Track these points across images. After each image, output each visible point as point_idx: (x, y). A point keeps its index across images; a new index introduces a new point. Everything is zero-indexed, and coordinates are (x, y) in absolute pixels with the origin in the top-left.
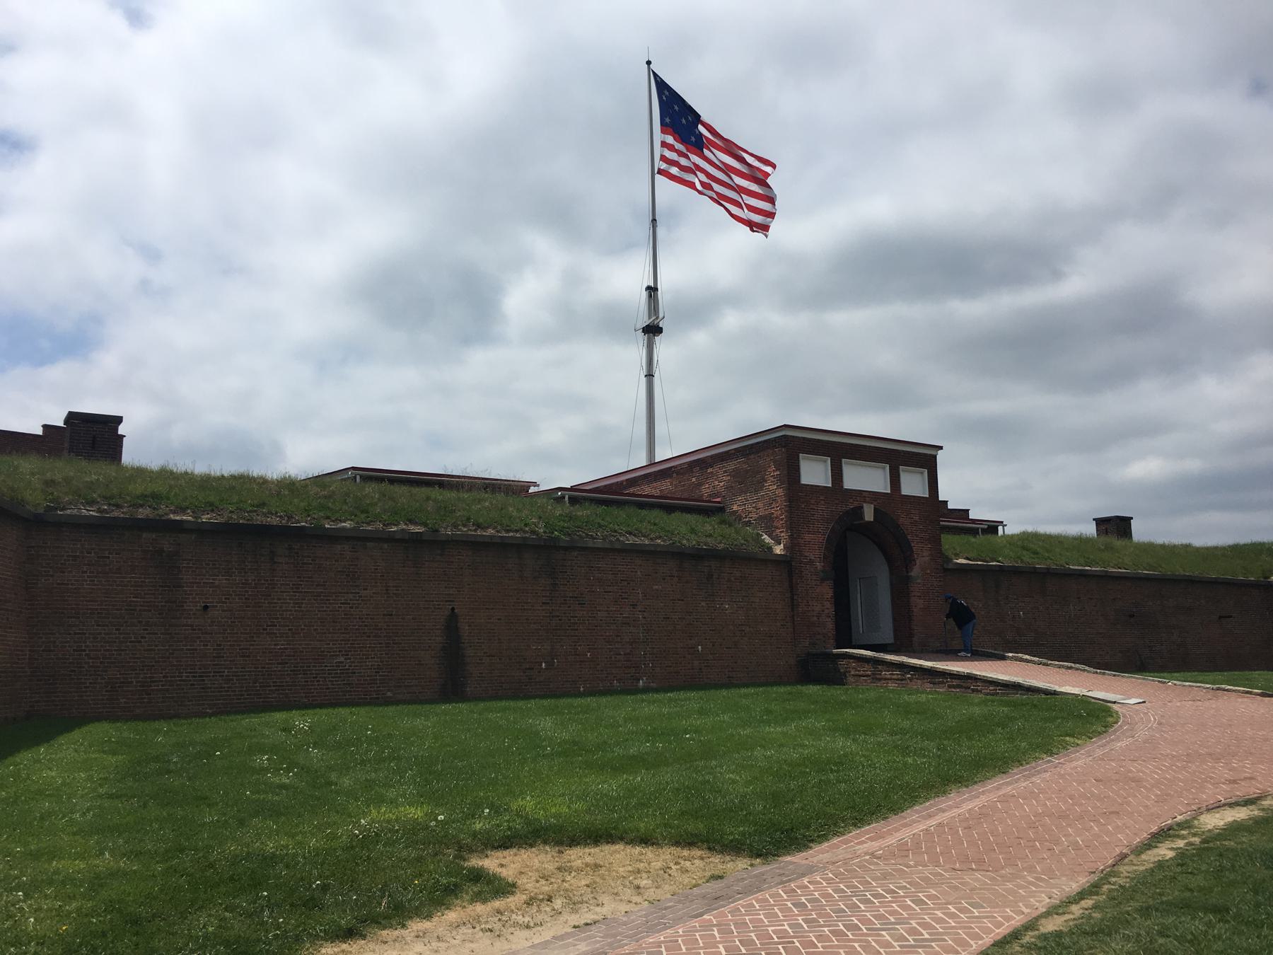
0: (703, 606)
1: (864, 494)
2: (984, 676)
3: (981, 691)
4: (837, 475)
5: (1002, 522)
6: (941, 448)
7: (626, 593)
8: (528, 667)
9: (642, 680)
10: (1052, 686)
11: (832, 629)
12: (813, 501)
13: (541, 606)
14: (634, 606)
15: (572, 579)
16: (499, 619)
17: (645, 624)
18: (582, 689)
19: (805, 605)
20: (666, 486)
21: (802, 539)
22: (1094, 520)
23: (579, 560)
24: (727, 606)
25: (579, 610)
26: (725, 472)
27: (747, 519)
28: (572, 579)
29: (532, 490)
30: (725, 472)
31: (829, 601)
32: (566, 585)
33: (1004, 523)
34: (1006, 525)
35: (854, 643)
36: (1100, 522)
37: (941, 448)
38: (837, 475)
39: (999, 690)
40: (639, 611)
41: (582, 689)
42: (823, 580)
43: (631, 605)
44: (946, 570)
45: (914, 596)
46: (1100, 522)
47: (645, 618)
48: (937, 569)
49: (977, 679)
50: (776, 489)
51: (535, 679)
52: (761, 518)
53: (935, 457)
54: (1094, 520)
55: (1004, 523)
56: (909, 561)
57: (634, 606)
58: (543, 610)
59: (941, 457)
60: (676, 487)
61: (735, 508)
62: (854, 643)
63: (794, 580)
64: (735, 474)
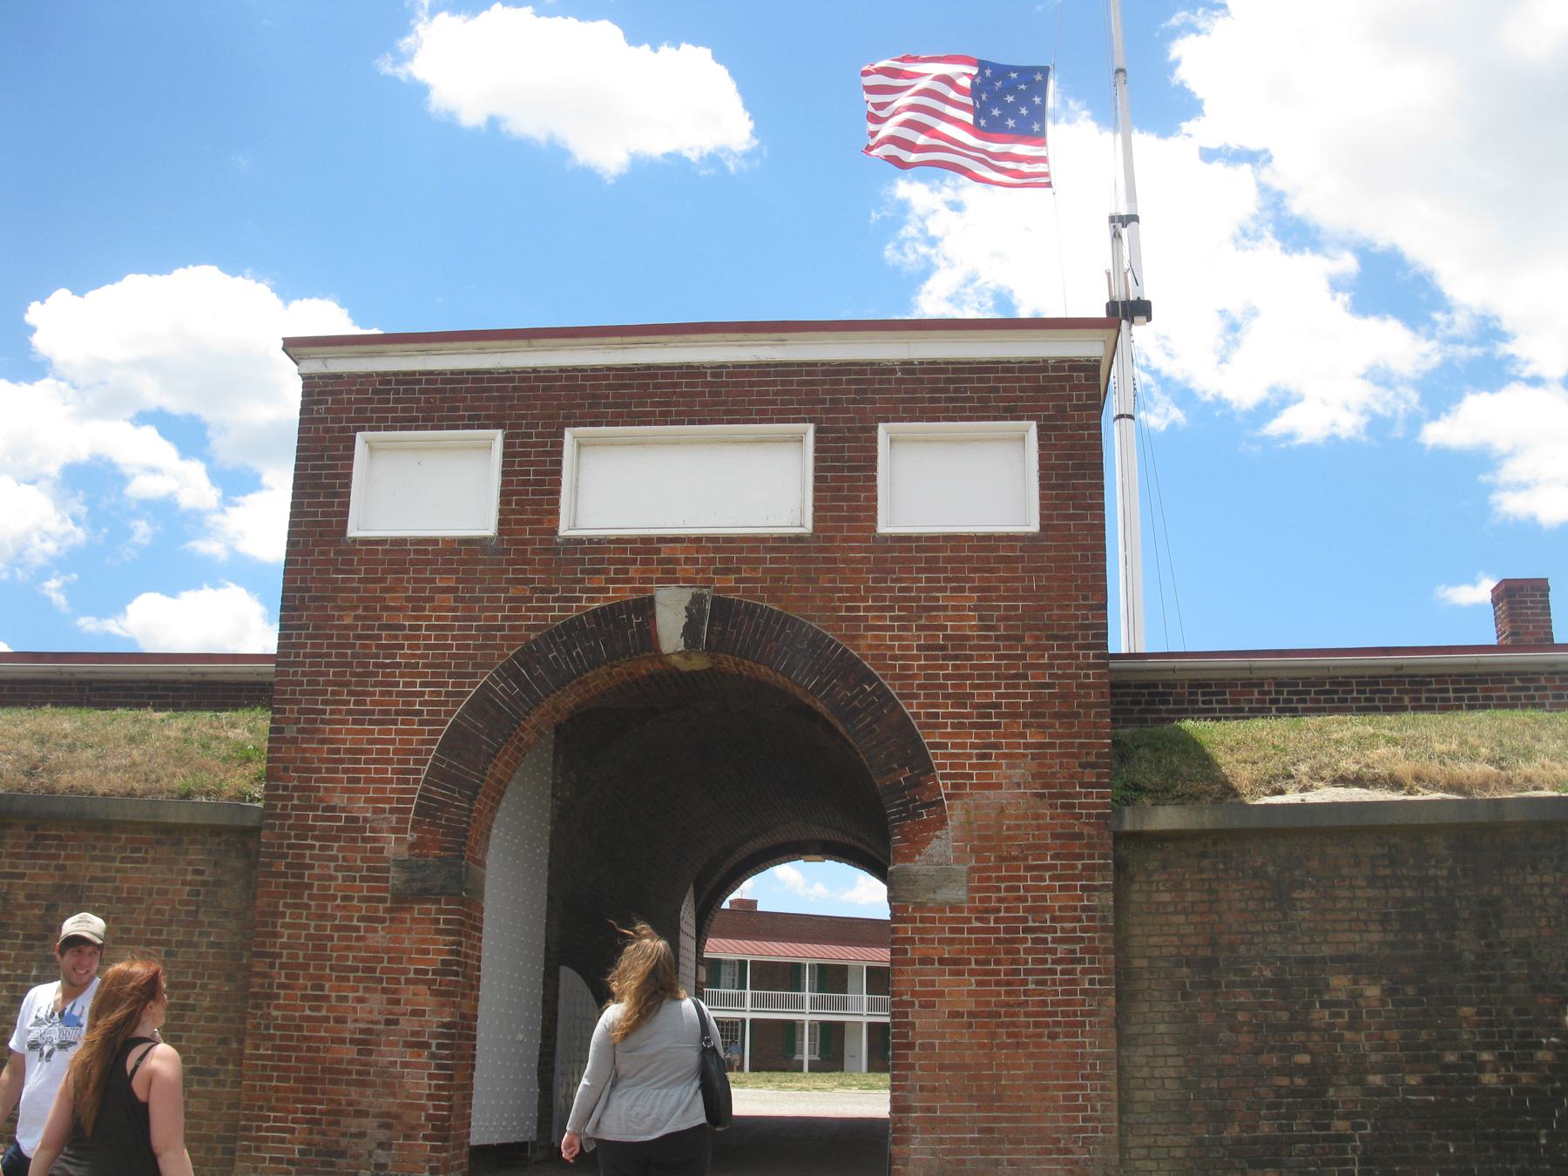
31: (429, 983)
45: (925, 961)
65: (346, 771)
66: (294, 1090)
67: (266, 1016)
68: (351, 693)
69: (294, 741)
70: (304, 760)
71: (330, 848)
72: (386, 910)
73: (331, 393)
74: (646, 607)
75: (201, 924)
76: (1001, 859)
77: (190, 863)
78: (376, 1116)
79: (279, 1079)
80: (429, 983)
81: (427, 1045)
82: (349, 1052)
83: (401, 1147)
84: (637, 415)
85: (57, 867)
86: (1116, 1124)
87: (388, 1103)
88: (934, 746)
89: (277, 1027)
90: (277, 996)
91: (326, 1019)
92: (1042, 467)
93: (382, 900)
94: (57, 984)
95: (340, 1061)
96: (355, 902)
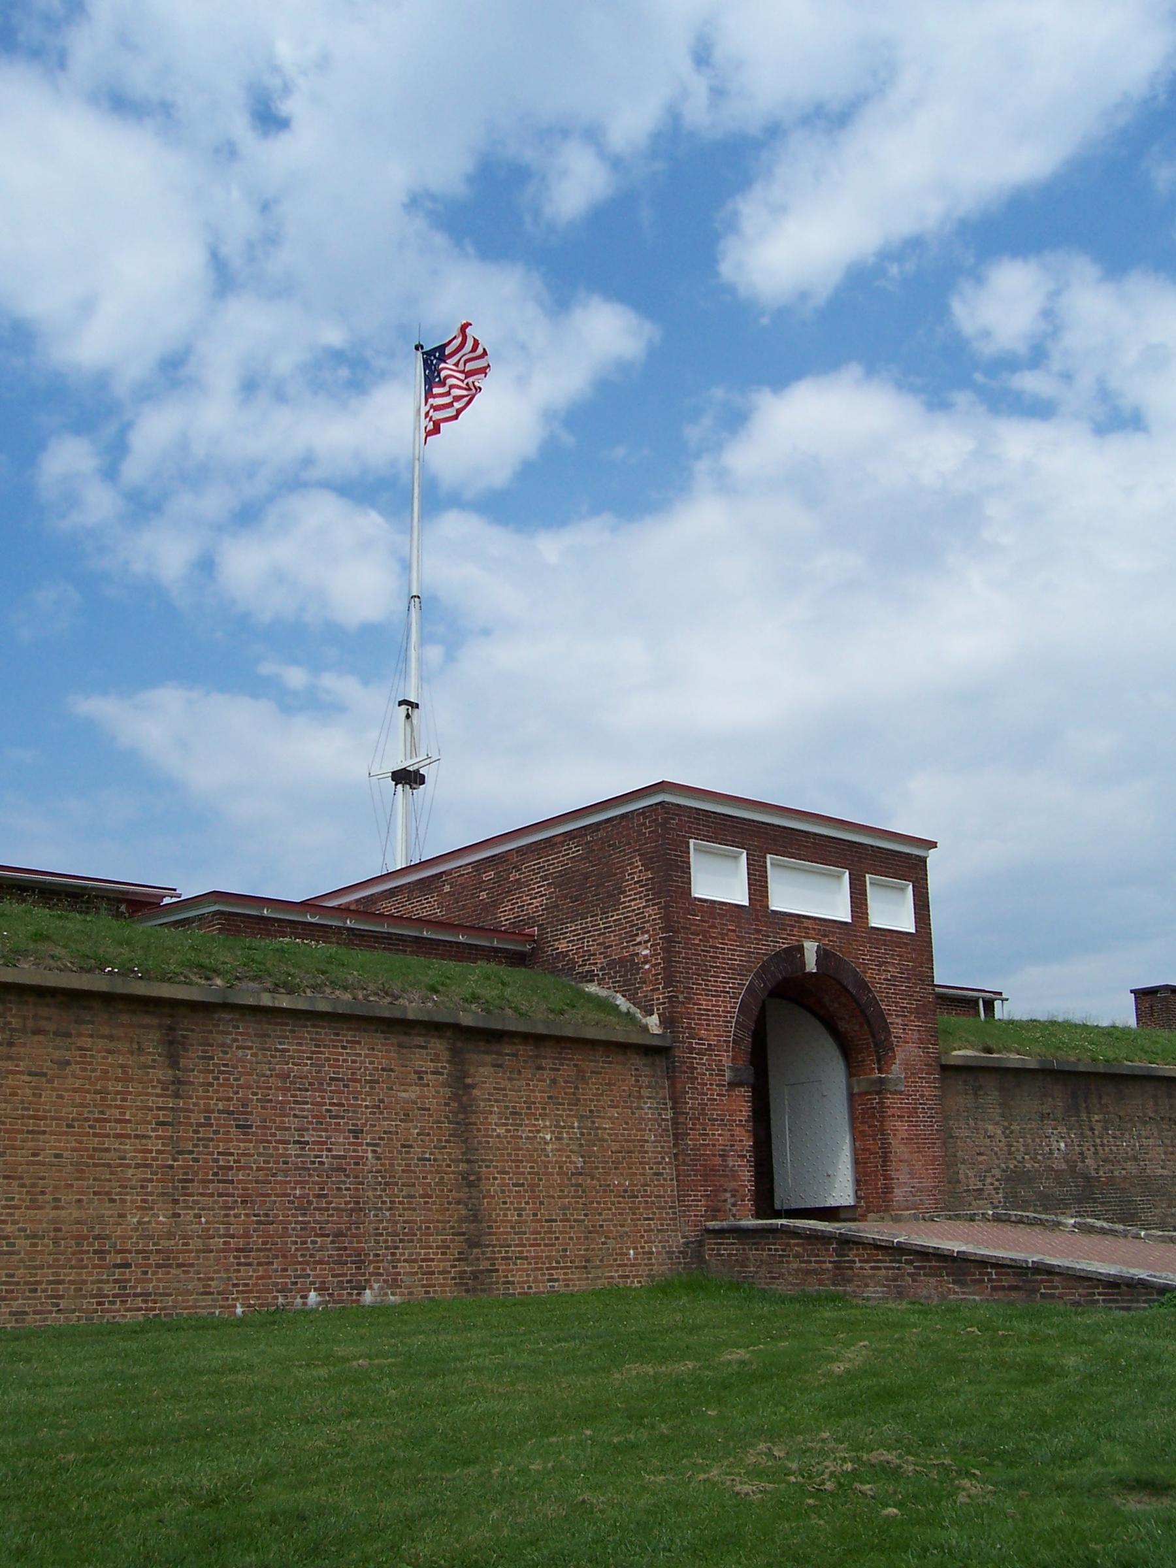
0: (498, 1136)
1: (807, 923)
2: (1068, 1268)
3: (1061, 1297)
4: (758, 885)
5: (1000, 994)
6: (933, 845)
7: (341, 1105)
8: (119, 1261)
9: (371, 1288)
10: (1125, 1269)
11: (749, 1181)
12: (714, 932)
13: (153, 1130)
14: (356, 1133)
15: (224, 1072)
16: (57, 1156)
17: (379, 1171)
18: (239, 1310)
19: (700, 1135)
20: (429, 907)
21: (694, 1004)
22: (1132, 991)
23: (241, 1034)
24: (548, 1137)
25: (239, 1140)
26: (544, 878)
27: (587, 968)
28: (224, 1072)
29: (167, 901)
30: (544, 878)
31: (744, 1126)
32: (211, 1085)
33: (1004, 996)
34: (1007, 1000)
35: (777, 1206)
36: (1144, 996)
37: (933, 845)
38: (758, 885)
39: (1100, 1294)
40: (368, 1144)
41: (239, 1310)
42: (732, 1085)
43: (350, 1131)
44: (945, 1068)
45: (893, 1116)
46: (1144, 996)
47: (378, 1158)
48: (930, 1065)
49: (927, 1254)
50: (644, 907)
51: (135, 1287)
52: (612, 964)
53: (923, 861)
54: (1132, 991)
55: (1004, 996)
56: (883, 1050)
57: (356, 1133)
58: (158, 1137)
59: (933, 858)
60: (448, 909)
61: (562, 946)
62: (777, 1206)
63: (679, 1086)
64: (563, 881)
65: (705, 1020)
66: (700, 1180)
67: (686, 1144)
68: (703, 980)
69: (683, 1003)
70: (688, 1013)
71: (702, 1059)
72: (726, 1090)
73: (677, 815)
74: (801, 949)
75: (643, 1098)
76: (912, 1074)
77: (633, 1064)
78: (731, 1191)
79: (695, 1175)
80: (744, 1126)
81: (745, 1156)
82: (718, 1161)
83: (740, 1205)
84: (789, 853)
85: (575, 1065)
86: (871, 1040)
87: (733, 1185)
88: (892, 1023)
89: (691, 1150)
90: (689, 1134)
91: (708, 1145)
92: (914, 895)
93: (724, 1086)
94: (1132, 1022)
95: (716, 1165)
96: (254, 1130)
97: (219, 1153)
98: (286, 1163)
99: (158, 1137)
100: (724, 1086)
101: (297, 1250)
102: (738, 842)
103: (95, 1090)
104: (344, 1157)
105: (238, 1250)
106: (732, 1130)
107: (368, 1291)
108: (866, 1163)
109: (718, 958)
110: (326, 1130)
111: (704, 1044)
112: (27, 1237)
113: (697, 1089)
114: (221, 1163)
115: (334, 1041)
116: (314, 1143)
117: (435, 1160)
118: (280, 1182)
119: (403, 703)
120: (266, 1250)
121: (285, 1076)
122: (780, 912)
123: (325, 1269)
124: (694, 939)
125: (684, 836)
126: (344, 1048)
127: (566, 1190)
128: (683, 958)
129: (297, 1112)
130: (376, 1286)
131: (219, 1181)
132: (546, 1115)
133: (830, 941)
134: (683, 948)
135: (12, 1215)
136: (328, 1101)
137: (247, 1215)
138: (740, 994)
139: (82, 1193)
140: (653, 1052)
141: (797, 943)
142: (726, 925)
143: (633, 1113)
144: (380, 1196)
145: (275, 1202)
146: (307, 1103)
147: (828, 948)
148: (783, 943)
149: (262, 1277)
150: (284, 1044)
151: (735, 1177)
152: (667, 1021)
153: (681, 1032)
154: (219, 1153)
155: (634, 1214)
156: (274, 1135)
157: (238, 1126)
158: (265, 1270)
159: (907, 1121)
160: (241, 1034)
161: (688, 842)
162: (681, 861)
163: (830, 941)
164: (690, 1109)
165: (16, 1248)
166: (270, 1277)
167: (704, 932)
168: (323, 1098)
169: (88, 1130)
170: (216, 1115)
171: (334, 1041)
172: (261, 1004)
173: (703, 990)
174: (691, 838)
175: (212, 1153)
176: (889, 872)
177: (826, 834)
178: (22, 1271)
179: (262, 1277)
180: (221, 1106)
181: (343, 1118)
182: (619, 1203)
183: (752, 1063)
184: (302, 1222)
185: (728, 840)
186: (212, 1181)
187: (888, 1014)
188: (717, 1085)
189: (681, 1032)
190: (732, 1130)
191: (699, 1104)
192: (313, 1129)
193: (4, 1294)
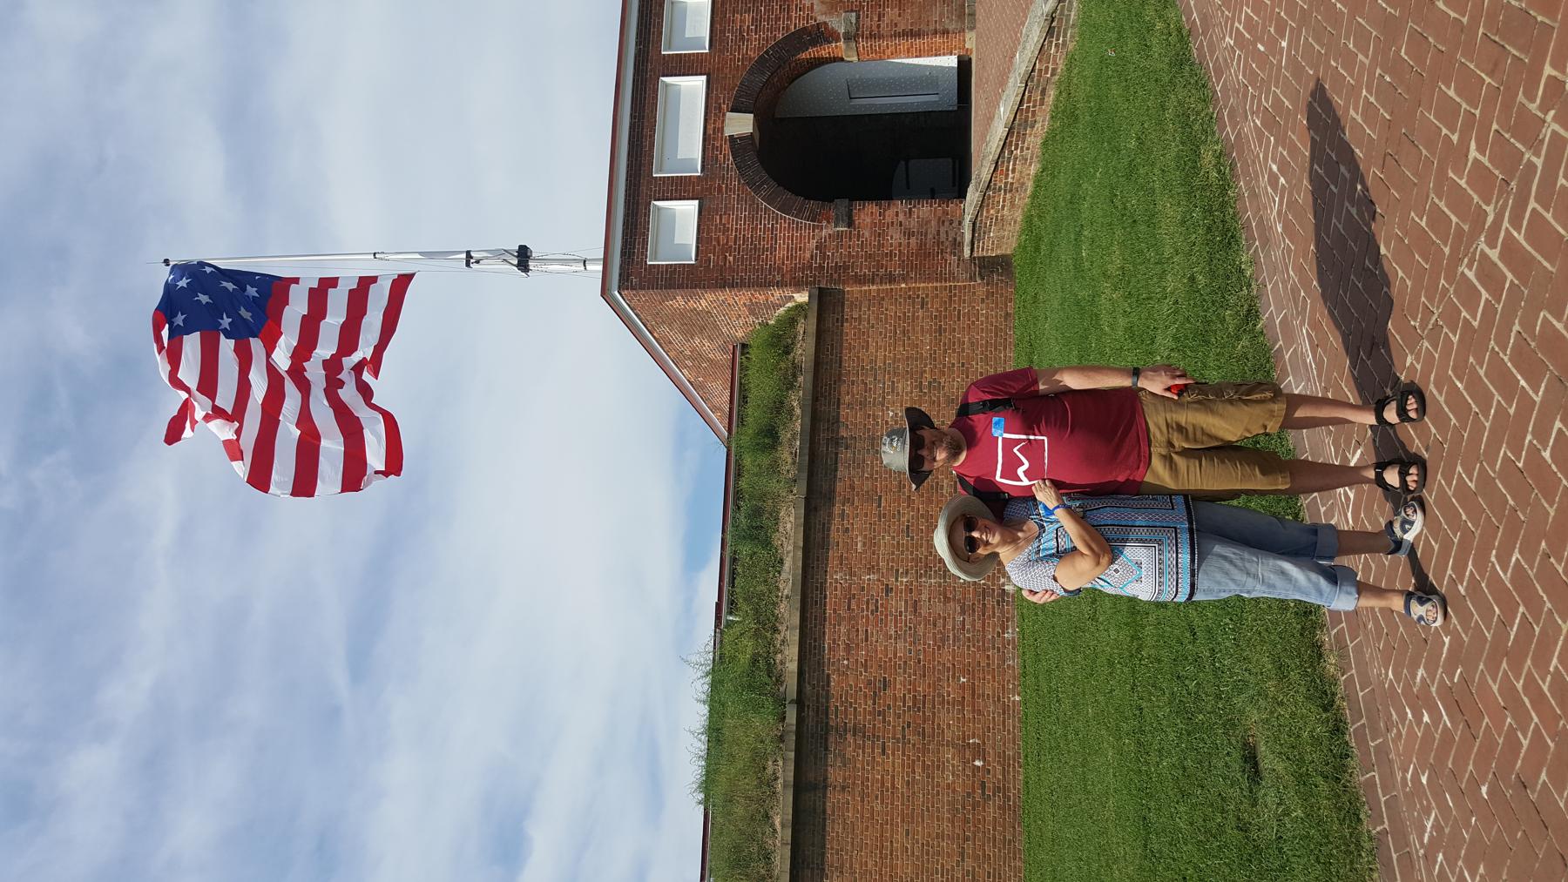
7: (868, 603)
9: (1003, 584)
12: (723, 240)
14: (888, 590)
15: (846, 698)
23: (818, 682)
28: (846, 698)
41: (1017, 698)
58: (893, 754)
69: (783, 275)
82: (913, 240)
88: (795, 28)
93: (850, 232)
97: (904, 706)
98: (910, 650)
99: (893, 754)
100: (850, 232)
101: (974, 646)
102: (646, 209)
103: (861, 801)
104: (906, 602)
105: (973, 696)
106: (888, 224)
107: (1006, 587)
108: (920, 50)
109: (744, 235)
110: (886, 616)
111: (816, 253)
112: (963, 860)
113: (853, 263)
114: (911, 704)
115: (821, 605)
116: (896, 627)
117: (908, 521)
118: (925, 657)
119: (468, 264)
120: (973, 671)
121: (848, 648)
122: (698, 222)
123: (989, 623)
124: (730, 262)
125: (645, 270)
126: (825, 598)
127: (933, 398)
128: (746, 275)
129: (874, 639)
130: (1002, 580)
131: (924, 707)
132: (874, 415)
133: (724, 103)
134: (737, 274)
135: (948, 870)
136: (865, 612)
137: (949, 686)
138: (774, 212)
139: (933, 816)
140: (827, 303)
141: (728, 143)
142: (716, 225)
143: (873, 327)
144: (935, 571)
145: (938, 661)
146: (867, 631)
147: (730, 105)
148: (728, 160)
149: (994, 677)
150: (824, 647)
151: (926, 222)
152: (798, 285)
153: (807, 278)
154: (904, 706)
155: (954, 330)
156: (890, 659)
157: (885, 690)
158: (988, 674)
159: (884, 10)
160: (818, 682)
161: (650, 265)
162: (666, 274)
163: (724, 103)
164: (869, 271)
165: (970, 869)
166: (994, 669)
167: (723, 251)
168: (863, 617)
169: (889, 809)
170: (876, 706)
171: (821, 605)
172: (796, 670)
173: (772, 254)
174: (646, 264)
175: (904, 711)
176: (658, 22)
177: (631, 91)
178: (986, 866)
179: (994, 677)
180: (870, 702)
181: (877, 600)
182: (945, 344)
183: (831, 201)
184: (954, 641)
185: (645, 219)
186: (924, 712)
187: (787, 32)
188: (850, 241)
189: (807, 278)
190: (888, 224)
191: (866, 261)
192: (886, 626)
193: (1002, 881)
